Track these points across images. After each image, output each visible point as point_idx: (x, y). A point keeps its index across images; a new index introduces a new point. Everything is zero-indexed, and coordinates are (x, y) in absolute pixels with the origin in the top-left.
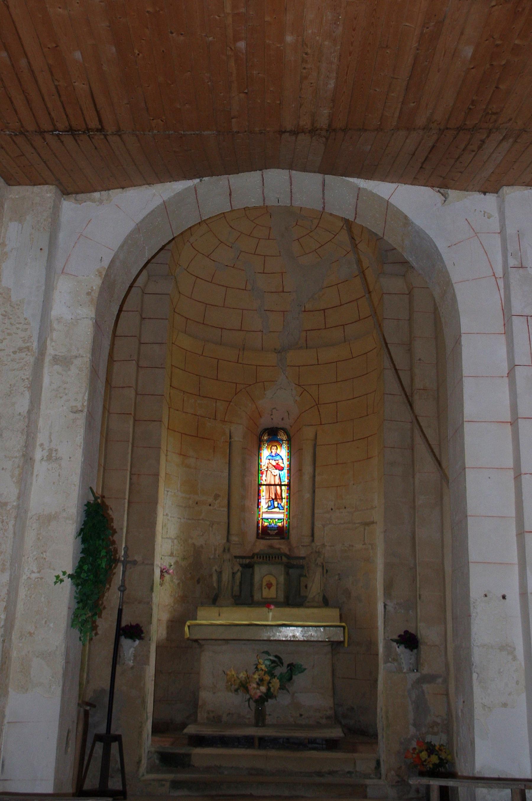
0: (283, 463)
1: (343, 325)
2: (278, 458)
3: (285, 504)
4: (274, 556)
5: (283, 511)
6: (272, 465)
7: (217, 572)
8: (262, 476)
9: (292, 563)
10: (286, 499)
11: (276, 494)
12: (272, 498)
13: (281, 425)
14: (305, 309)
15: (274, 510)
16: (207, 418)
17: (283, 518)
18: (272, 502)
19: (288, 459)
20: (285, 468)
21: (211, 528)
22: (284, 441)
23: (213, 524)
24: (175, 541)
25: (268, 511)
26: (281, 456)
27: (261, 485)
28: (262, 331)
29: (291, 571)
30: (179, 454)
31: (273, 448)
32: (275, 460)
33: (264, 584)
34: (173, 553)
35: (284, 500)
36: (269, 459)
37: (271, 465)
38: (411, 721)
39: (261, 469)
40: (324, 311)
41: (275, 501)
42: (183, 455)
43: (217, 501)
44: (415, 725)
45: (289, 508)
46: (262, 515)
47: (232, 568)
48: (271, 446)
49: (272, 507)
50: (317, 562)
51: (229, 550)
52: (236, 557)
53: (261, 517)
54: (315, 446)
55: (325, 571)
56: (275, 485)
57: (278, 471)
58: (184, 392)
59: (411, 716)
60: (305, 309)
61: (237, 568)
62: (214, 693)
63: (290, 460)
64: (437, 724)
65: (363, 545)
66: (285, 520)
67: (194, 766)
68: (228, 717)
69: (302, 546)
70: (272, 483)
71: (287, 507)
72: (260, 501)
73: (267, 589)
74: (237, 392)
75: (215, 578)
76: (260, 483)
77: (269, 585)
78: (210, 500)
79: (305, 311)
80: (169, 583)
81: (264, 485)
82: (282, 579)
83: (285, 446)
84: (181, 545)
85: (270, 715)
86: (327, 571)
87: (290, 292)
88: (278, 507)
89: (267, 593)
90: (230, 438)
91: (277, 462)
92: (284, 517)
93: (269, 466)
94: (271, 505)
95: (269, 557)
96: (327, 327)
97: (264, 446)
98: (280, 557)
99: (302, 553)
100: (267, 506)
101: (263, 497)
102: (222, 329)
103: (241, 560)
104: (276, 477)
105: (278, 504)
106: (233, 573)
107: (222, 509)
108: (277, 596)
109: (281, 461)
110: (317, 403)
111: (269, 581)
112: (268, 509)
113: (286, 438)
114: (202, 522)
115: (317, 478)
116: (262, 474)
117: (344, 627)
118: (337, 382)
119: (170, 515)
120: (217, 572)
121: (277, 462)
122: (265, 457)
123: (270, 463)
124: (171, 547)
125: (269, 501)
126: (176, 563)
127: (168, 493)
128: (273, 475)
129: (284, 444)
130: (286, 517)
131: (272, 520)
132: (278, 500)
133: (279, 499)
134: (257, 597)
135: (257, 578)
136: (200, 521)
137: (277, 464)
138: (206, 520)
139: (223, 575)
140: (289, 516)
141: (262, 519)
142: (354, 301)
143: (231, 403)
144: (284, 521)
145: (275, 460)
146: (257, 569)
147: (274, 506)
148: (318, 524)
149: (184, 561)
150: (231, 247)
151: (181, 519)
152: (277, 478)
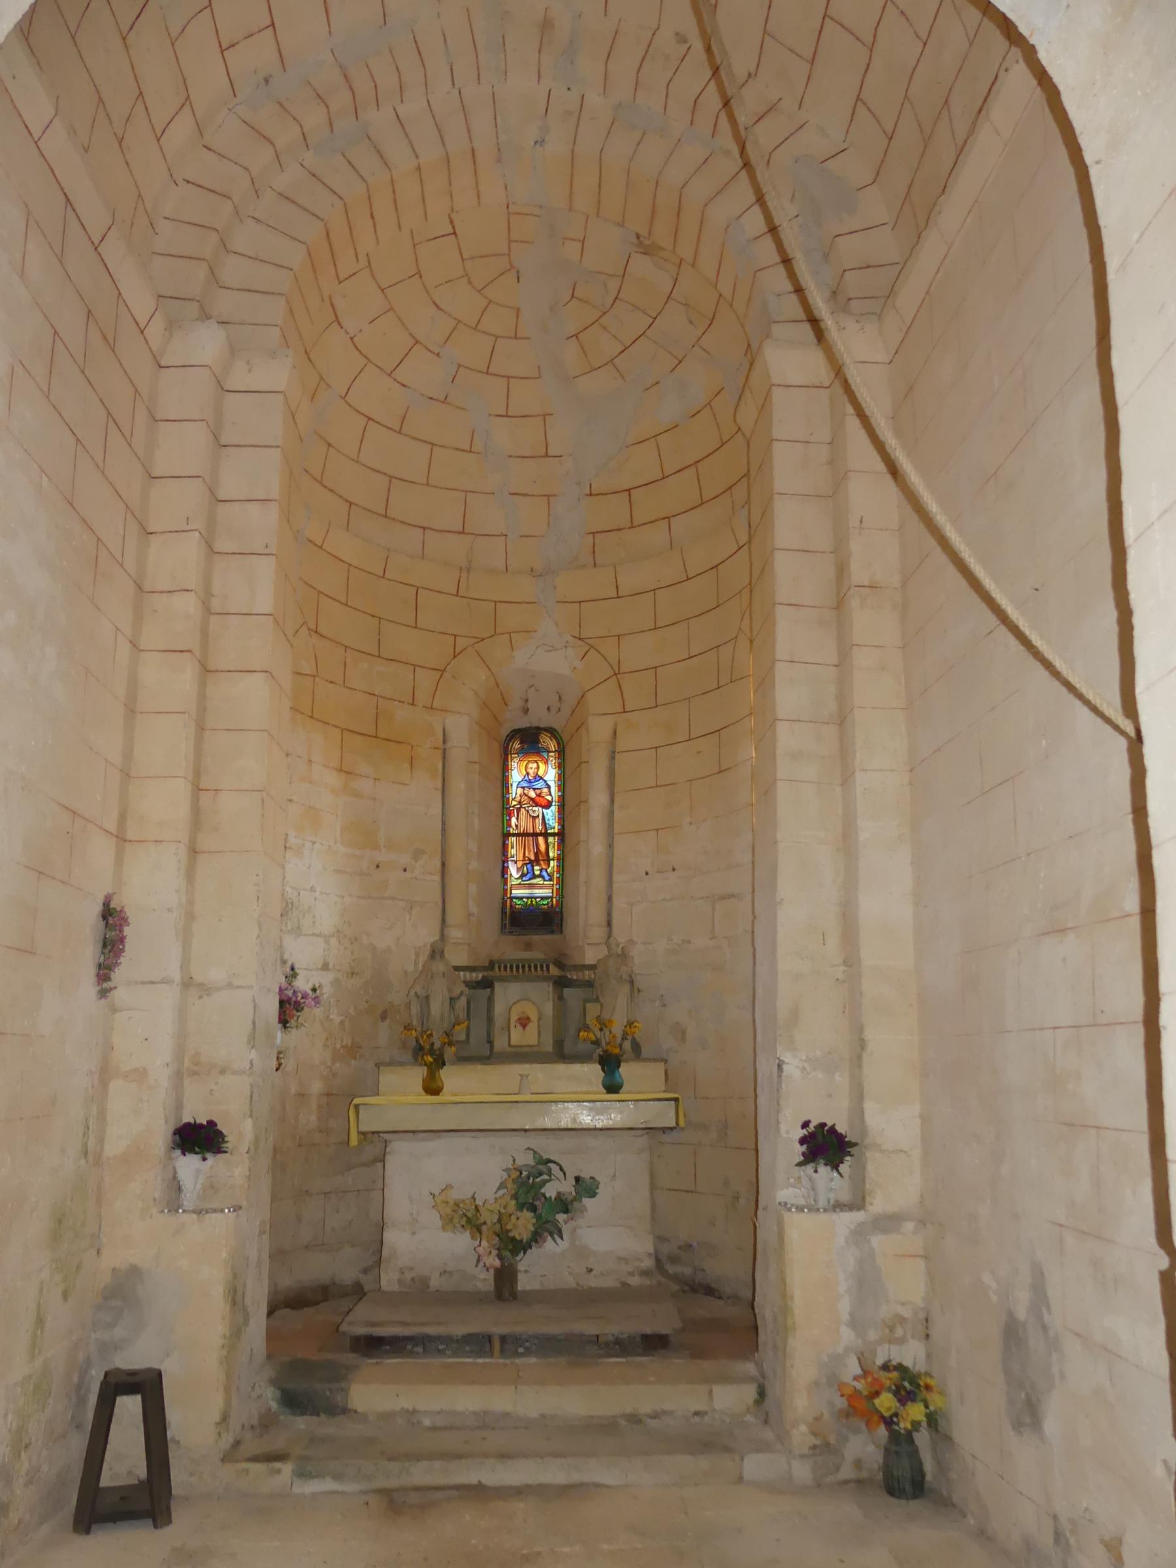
0: (550, 795)
1: (666, 518)
2: (540, 784)
3: (555, 869)
4: (532, 965)
5: (552, 883)
6: (529, 797)
7: (418, 997)
8: (510, 820)
9: (569, 976)
10: (556, 861)
12: (529, 859)
13: (545, 720)
14: (591, 491)
16: (396, 700)
17: (551, 894)
18: (529, 866)
19: (559, 786)
20: (554, 804)
22: (552, 752)
24: (333, 941)
25: (522, 883)
26: (545, 781)
27: (509, 835)
28: (506, 535)
29: (566, 991)
30: (336, 769)
31: (530, 765)
32: (534, 789)
33: (514, 1018)
34: (329, 965)
35: (552, 862)
36: (523, 788)
37: (526, 798)
38: (845, 1317)
39: (508, 806)
40: (629, 492)
41: (535, 864)
42: (347, 772)
44: (853, 1324)
45: (564, 772)
46: (511, 890)
48: (526, 762)
49: (529, 876)
51: (442, 953)
52: (457, 969)
53: (508, 896)
54: (612, 756)
55: (636, 991)
56: (535, 835)
57: (540, 809)
58: (346, 647)
59: (844, 1307)
60: (591, 491)
61: (460, 988)
62: (414, 1233)
63: (562, 787)
64: (902, 1320)
65: (711, 939)
66: (554, 900)
67: (356, 1412)
68: (442, 1279)
70: (528, 832)
71: (558, 875)
72: (506, 865)
73: (520, 1028)
74: (456, 654)
75: (415, 1009)
76: (505, 832)
77: (524, 1022)
78: (405, 860)
79: (591, 495)
80: (322, 1023)
81: (514, 835)
82: (549, 1009)
83: (554, 761)
84: (345, 948)
85: (526, 1271)
86: (639, 991)
87: (561, 456)
88: (540, 876)
89: (517, 1036)
90: (444, 742)
91: (538, 792)
92: (552, 893)
93: (522, 800)
95: (523, 967)
96: (635, 523)
97: (513, 763)
98: (544, 965)
99: (591, 956)
100: (520, 873)
102: (424, 530)
103: (468, 974)
104: (537, 820)
105: (541, 870)
106: (451, 999)
108: (539, 1042)
109: (545, 790)
110: (617, 672)
111: (524, 1012)
112: (523, 881)
113: (555, 746)
115: (618, 815)
116: (510, 815)
117: (676, 1100)
118: (655, 628)
119: (318, 889)
120: (418, 997)
121: (538, 792)
122: (515, 785)
123: (524, 794)
124: (324, 951)
125: (524, 864)
126: (336, 982)
127: (315, 846)
128: (530, 815)
129: (551, 758)
130: (557, 894)
132: (542, 862)
133: (543, 860)
134: (500, 1044)
135: (499, 1008)
137: (539, 795)
139: (432, 1003)
140: (561, 893)
141: (511, 898)
142: (691, 465)
143: (446, 674)
144: (552, 901)
145: (534, 789)
147: (534, 873)
148: (619, 903)
150: (438, 355)
151: (343, 897)
152: (539, 822)
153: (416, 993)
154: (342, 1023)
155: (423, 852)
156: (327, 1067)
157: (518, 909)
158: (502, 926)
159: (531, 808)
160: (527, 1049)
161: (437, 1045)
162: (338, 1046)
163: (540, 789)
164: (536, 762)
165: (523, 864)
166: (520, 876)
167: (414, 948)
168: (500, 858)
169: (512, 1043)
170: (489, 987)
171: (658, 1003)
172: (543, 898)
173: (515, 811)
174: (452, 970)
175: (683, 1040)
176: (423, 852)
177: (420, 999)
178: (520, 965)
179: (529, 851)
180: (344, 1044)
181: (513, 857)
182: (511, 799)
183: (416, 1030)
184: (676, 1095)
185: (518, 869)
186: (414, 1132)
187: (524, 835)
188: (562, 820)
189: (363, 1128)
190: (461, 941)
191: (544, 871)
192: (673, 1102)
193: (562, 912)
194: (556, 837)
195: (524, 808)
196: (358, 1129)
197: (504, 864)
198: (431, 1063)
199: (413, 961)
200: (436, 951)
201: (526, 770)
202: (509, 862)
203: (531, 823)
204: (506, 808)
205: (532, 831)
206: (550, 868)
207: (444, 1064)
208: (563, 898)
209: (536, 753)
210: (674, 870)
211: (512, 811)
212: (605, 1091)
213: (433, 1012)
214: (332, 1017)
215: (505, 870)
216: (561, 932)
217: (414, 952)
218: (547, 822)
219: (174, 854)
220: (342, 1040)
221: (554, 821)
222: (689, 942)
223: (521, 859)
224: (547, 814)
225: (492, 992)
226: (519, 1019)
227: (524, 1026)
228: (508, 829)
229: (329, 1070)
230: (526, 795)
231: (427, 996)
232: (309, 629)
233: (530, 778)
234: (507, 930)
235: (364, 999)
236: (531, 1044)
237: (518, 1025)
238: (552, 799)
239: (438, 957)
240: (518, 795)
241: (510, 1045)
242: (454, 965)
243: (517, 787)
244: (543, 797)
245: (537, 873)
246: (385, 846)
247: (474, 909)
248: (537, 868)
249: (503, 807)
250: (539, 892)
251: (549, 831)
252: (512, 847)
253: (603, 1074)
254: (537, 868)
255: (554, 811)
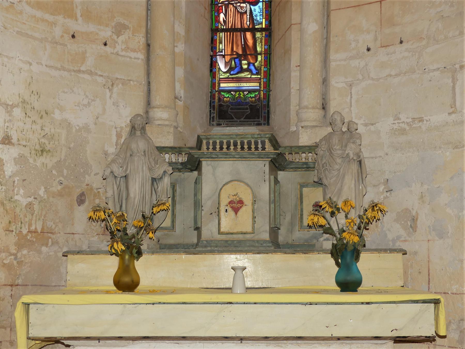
5: (259, 76)
7: (115, 177)
8: (219, 16)
11: (245, 47)
12: (237, 54)
15: (242, 75)
17: (258, 88)
18: (237, 60)
21: (108, 90)
23: (113, 85)
24: (17, 112)
33: (224, 201)
35: (259, 58)
39: (216, 3)
43: (122, 38)
47: (150, 169)
49: (236, 70)
50: (347, 152)
52: (161, 149)
56: (243, 30)
57: (248, 5)
66: (262, 92)
69: (302, 127)
71: (266, 69)
73: (231, 213)
76: (214, 27)
78: (106, 33)
81: (223, 30)
88: (248, 70)
92: (260, 86)
94: (236, 67)
101: (219, 52)
104: (245, 16)
105: (249, 64)
106: (154, 180)
107: (133, 55)
108: (253, 228)
114: (87, 76)
117: (436, 302)
128: (238, 11)
131: (238, 93)
132: (249, 56)
133: (251, 55)
136: (81, 75)
138: (96, 74)
141: (220, 91)
144: (259, 94)
146: (206, 166)
147: (241, 67)
149: (42, 155)
151: (31, 64)
152: (246, 18)
153: (112, 172)
154: (30, 205)
155: (125, 27)
156: (11, 254)
157: (227, 102)
158: (210, 119)
159: (239, 4)
160: (241, 237)
161: (131, 231)
162: (25, 231)
165: (231, 60)
167: (116, 128)
168: (208, 53)
169: (222, 230)
170: (195, 170)
171: (382, 188)
172: (250, 91)
173: (224, 7)
174: (157, 153)
175: (414, 228)
176: (125, 27)
177: (119, 179)
178: (232, 141)
179: (237, 46)
180: (33, 228)
181: (222, 52)
183: (105, 212)
184: (437, 297)
185: (226, 64)
186: (99, 339)
187: (233, 30)
188: (269, 16)
189: (34, 333)
190: (167, 123)
191: (251, 65)
192: (433, 305)
193: (268, 106)
194: (264, 33)
195: (232, 4)
196: (28, 333)
197: (212, 59)
198: (123, 251)
199: (115, 144)
200: (136, 126)
203: (239, 19)
205: (239, 27)
206: (258, 62)
207: (140, 253)
210: (401, 42)
211: (221, 8)
212: (338, 288)
213: (132, 195)
214: (16, 197)
215: (213, 65)
216: (268, 124)
217: (115, 133)
219: (57, 152)
220: (30, 225)
221: (261, 17)
222: (421, 120)
223: (229, 53)
224: (255, 10)
225: (200, 174)
226: (230, 203)
227: (236, 210)
229: (13, 257)
231: (126, 176)
234: (215, 123)
235: (58, 180)
236: (244, 230)
237: (230, 210)
239: (138, 133)
241: (220, 233)
242: (158, 145)
245: (245, 67)
246: (81, 16)
247: (180, 90)
248: (244, 62)
250: (246, 85)
251: (256, 27)
252: (221, 42)
253: (337, 269)
254: (244, 62)
255: (261, 7)
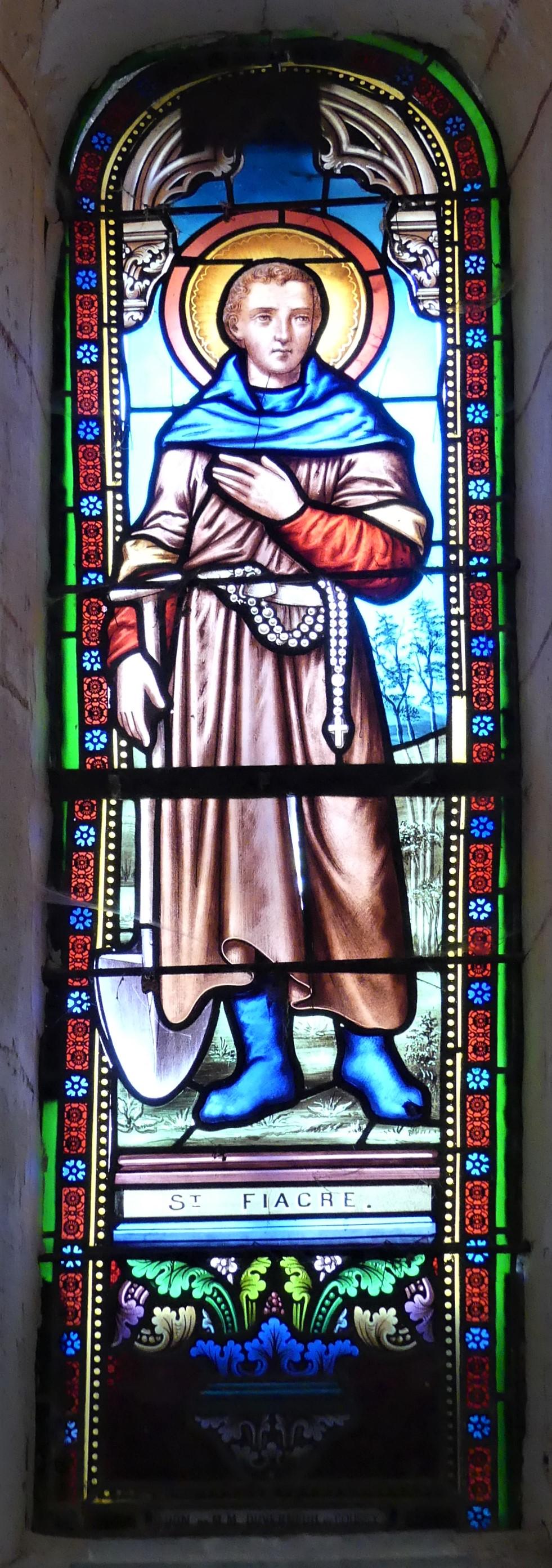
5: (431, 1135)
8: (110, 674)
17: (425, 1226)
20: (436, 557)
22: (419, 202)
25: (200, 1136)
26: (373, 406)
37: (229, 518)
41: (296, 996)
46: (114, 1192)
70: (246, 761)
92: (437, 1213)
93: (201, 535)
123: (215, 488)
128: (261, 641)
133: (360, 967)
144: (433, 1272)
147: (290, 1066)
163: (335, 455)
164: (302, 270)
166: (188, 1083)
173: (149, 609)
179: (256, 900)
181: (134, 946)
182: (112, 529)
191: (367, 1046)
201: (224, 329)
202: (106, 985)
204: (83, 593)
206: (417, 1024)
208: (518, 1246)
209: (303, 207)
211: (126, 615)
218: (389, 689)
224: (388, 630)
228: (97, 740)
230: (229, 502)
232: (179, 412)
233: (258, 379)
238: (426, 531)
240: (167, 502)
243: (162, 448)
244: (357, 513)
249: (56, 585)
251: (401, 758)
